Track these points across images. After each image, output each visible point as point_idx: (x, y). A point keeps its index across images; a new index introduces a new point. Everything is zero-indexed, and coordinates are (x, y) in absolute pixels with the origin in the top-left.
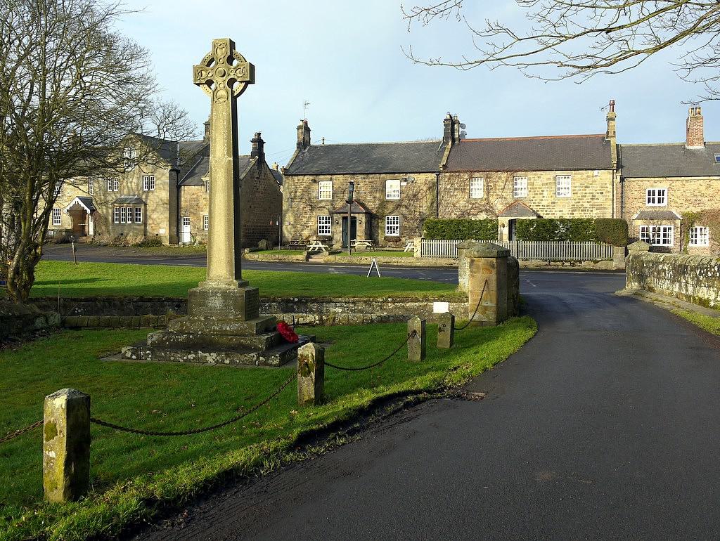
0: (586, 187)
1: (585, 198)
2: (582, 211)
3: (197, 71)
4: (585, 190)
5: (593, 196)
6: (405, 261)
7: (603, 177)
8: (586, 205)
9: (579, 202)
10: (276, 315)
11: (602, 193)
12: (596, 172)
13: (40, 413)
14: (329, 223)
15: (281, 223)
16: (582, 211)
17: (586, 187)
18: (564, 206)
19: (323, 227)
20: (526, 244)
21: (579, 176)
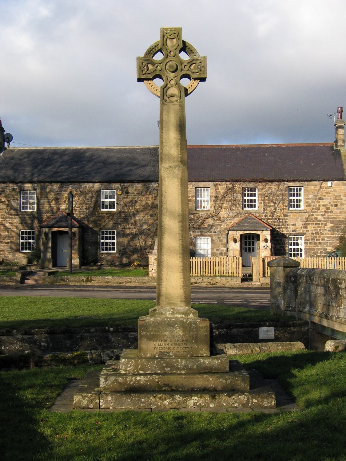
0: (320, 199)
1: (319, 211)
2: (316, 224)
3: (177, 33)
4: (319, 202)
5: (327, 209)
6: (78, 232)
7: (337, 189)
8: (320, 218)
9: (312, 215)
10: (6, 373)
11: (336, 205)
12: (329, 183)
13: (154, 206)
14: (255, 196)
15: (139, 149)
16: (316, 224)
17: (320, 199)
18: (297, 220)
19: (251, 196)
20: (196, 260)
21: (312, 187)
